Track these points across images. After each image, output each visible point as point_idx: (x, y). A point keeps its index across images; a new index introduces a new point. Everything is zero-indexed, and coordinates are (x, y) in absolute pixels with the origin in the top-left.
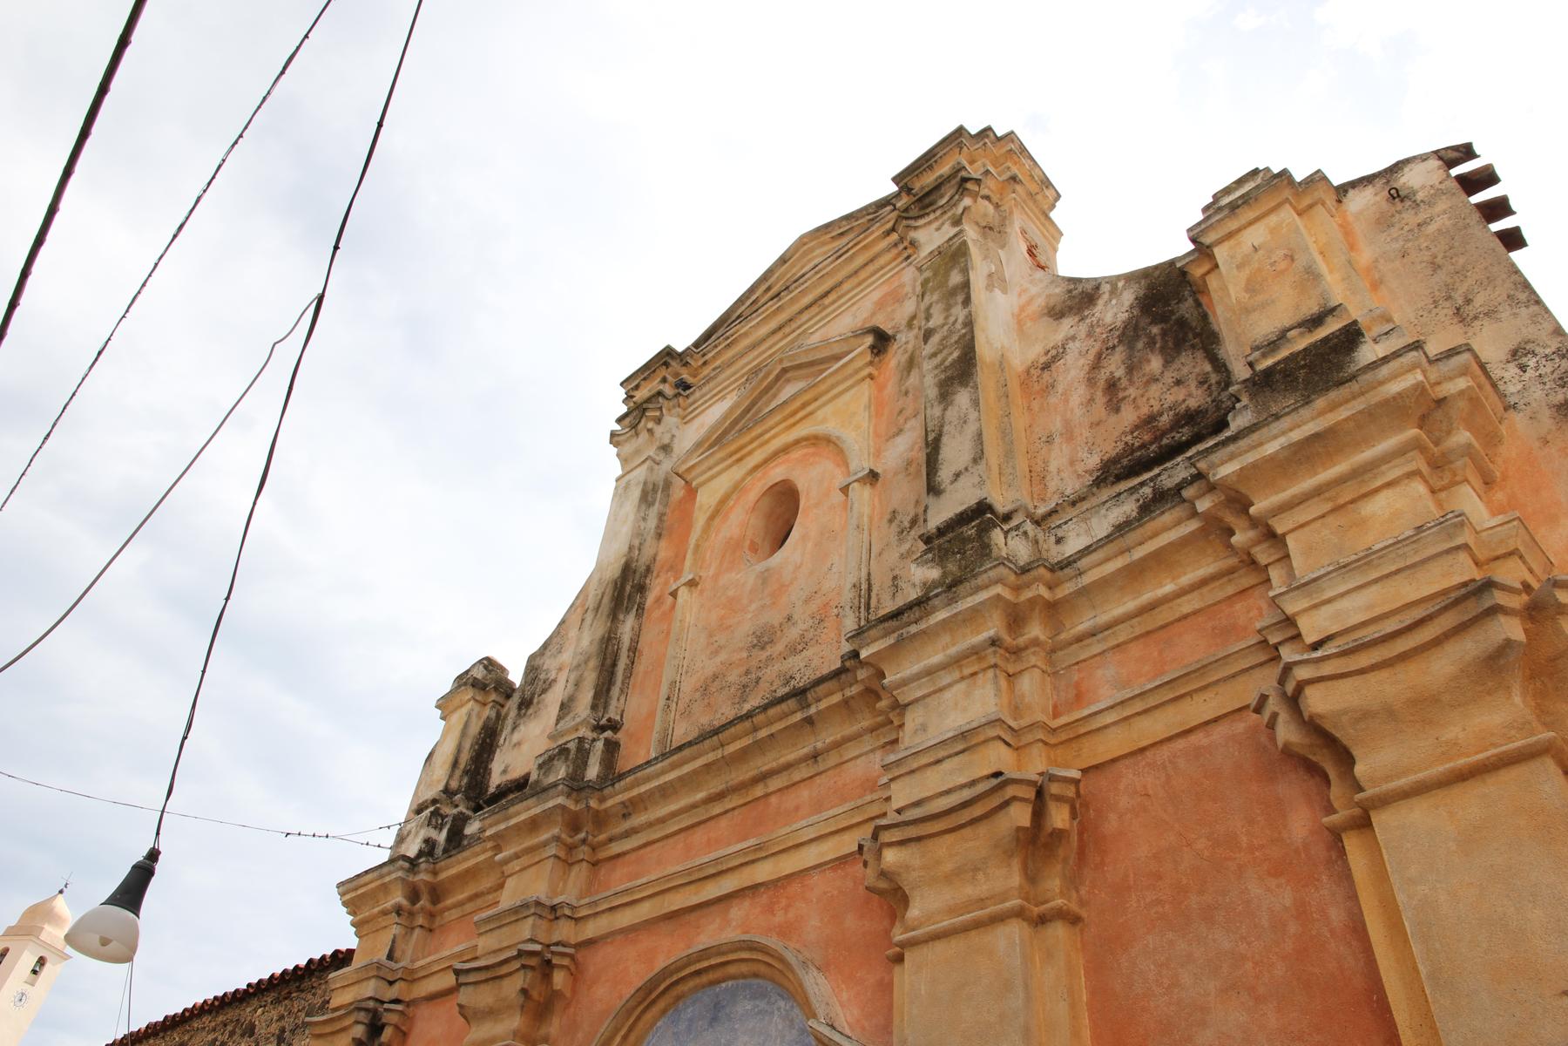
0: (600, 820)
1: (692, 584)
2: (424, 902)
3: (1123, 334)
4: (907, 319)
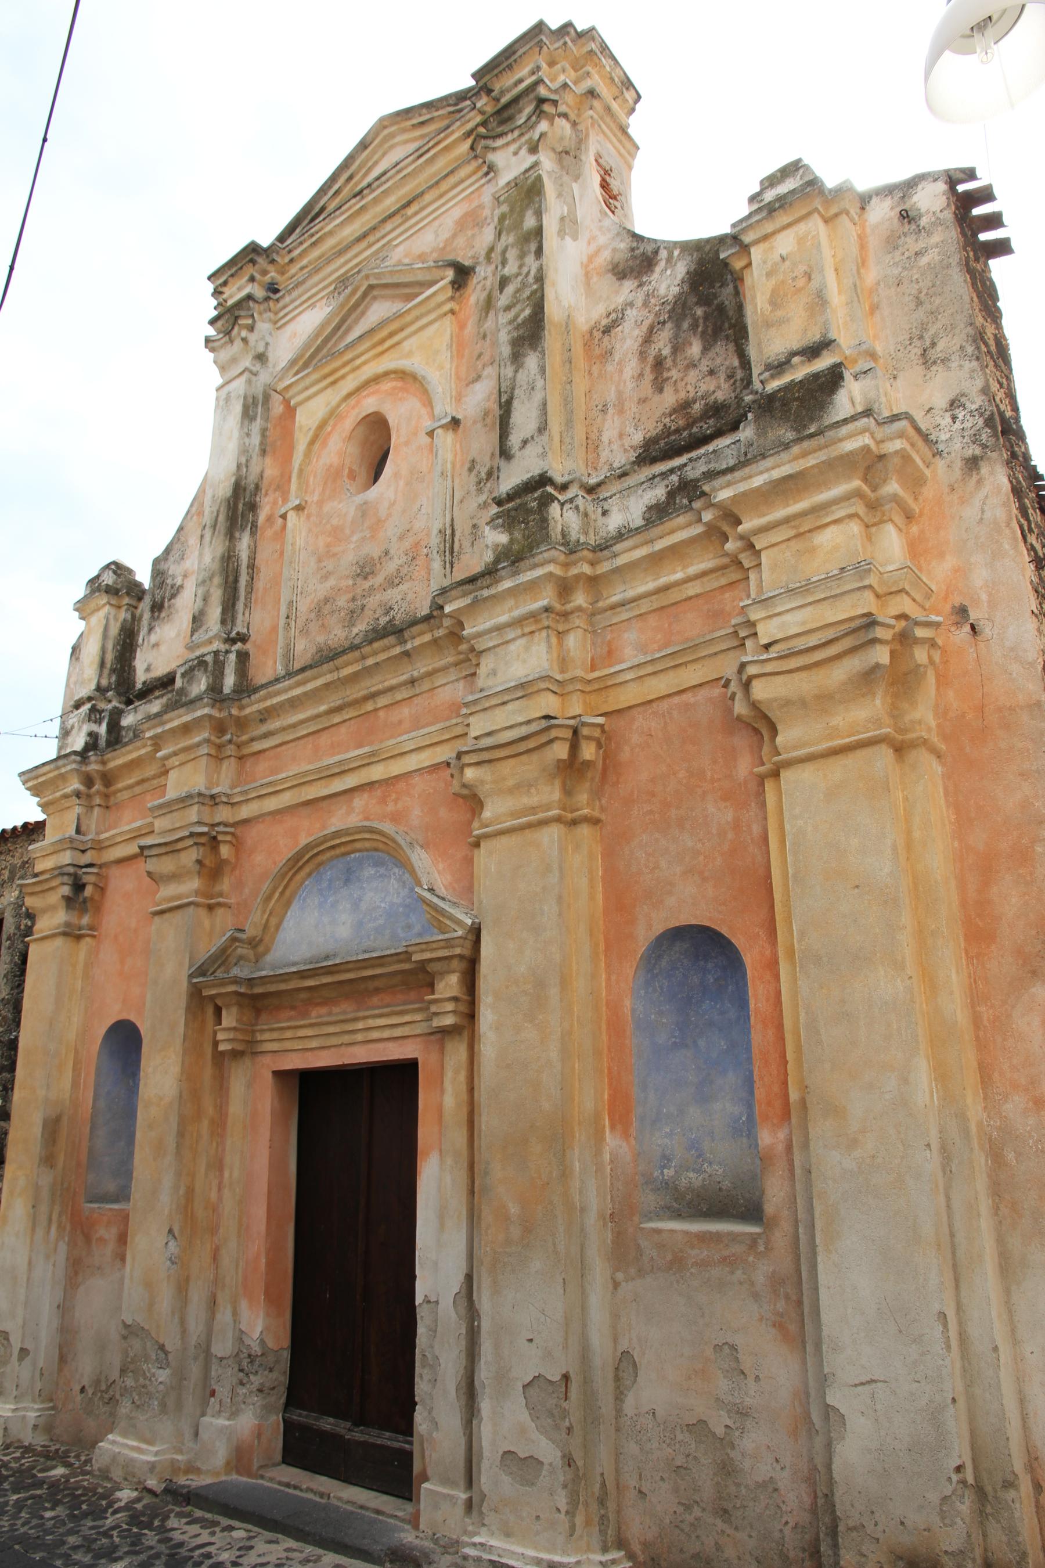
0: (241, 724)
1: (299, 508)
2: (98, 786)
3: (673, 310)
4: (486, 250)
